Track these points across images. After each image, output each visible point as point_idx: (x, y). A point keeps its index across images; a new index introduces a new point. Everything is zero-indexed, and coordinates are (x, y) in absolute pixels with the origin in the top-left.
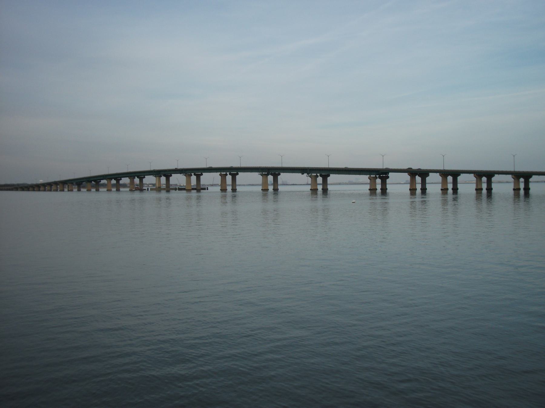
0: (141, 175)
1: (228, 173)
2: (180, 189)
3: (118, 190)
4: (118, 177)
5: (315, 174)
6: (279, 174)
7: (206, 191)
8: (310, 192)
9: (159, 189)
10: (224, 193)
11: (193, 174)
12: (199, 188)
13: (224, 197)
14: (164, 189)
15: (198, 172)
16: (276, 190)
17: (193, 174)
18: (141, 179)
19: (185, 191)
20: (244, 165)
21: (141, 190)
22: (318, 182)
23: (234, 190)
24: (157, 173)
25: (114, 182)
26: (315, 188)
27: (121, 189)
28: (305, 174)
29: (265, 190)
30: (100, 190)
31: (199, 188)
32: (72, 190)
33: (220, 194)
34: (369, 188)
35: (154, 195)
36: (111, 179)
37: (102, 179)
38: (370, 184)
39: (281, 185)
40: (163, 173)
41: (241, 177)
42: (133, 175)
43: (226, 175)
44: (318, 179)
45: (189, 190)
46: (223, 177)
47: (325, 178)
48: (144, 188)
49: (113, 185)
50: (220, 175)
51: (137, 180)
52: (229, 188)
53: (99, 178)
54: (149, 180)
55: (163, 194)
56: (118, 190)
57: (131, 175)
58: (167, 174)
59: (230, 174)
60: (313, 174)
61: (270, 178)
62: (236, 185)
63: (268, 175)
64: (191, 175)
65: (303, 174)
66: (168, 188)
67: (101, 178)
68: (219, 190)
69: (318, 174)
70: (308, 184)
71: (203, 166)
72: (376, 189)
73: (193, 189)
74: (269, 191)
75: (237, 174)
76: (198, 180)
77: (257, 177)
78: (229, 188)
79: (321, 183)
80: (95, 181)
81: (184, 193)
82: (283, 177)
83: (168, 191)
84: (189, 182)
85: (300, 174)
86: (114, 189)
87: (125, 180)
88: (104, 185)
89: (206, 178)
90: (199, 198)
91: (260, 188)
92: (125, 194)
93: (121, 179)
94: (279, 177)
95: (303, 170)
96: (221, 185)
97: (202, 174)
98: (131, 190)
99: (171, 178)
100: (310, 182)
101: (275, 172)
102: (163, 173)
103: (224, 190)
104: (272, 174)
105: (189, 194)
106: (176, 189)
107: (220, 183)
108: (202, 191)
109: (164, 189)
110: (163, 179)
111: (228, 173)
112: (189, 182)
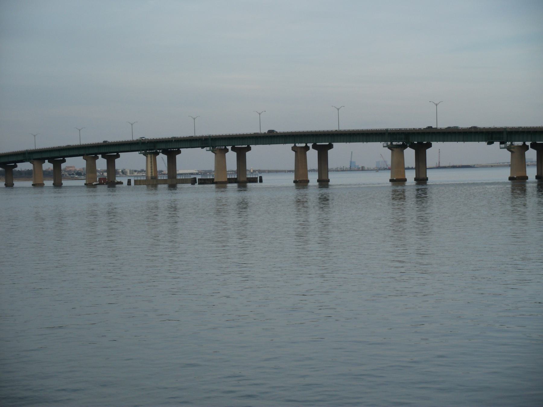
0: (111, 150)
1: (310, 145)
2: (203, 182)
3: (58, 185)
4: (57, 155)
5: (520, 143)
6: (429, 145)
7: (258, 184)
9: (152, 182)
11: (229, 148)
12: (242, 179)
15: (242, 143)
17: (229, 148)
19: (213, 186)
20: (443, 124)
22: (98, 168)
24: (149, 147)
25: (47, 166)
26: (520, 174)
27: (17, 184)
28: (497, 144)
29: (398, 181)
31: (243, 180)
33: (293, 193)
34: (389, 177)
35: (142, 197)
36: (42, 160)
37: (22, 161)
38: (511, 165)
39: (337, 170)
40: (163, 146)
42: (91, 151)
43: (307, 148)
44: (308, 153)
45: (221, 184)
47: (421, 152)
48: (118, 179)
49: (47, 175)
50: (294, 149)
51: (101, 163)
52: (313, 178)
53: (14, 159)
54: (131, 162)
56: (58, 185)
57: (89, 151)
58: (171, 147)
59: (233, 149)
61: (410, 154)
62: (327, 170)
63: (404, 147)
64: (227, 150)
65: (490, 143)
66: (173, 181)
68: (52, 185)
69: (528, 143)
72: (527, 178)
73: (231, 181)
74: (407, 183)
77: (379, 151)
78: (313, 178)
79: (413, 165)
83: (172, 187)
84: (221, 163)
85: (484, 144)
86: (49, 183)
87: (77, 163)
88: (27, 175)
89: (258, 157)
90: (243, 205)
91: (386, 176)
92: (75, 198)
93: (64, 161)
94: (428, 151)
95: (490, 135)
101: (419, 140)
104: (412, 146)
105: (220, 195)
108: (249, 185)
109: (164, 182)
111: (310, 145)
112: (221, 163)
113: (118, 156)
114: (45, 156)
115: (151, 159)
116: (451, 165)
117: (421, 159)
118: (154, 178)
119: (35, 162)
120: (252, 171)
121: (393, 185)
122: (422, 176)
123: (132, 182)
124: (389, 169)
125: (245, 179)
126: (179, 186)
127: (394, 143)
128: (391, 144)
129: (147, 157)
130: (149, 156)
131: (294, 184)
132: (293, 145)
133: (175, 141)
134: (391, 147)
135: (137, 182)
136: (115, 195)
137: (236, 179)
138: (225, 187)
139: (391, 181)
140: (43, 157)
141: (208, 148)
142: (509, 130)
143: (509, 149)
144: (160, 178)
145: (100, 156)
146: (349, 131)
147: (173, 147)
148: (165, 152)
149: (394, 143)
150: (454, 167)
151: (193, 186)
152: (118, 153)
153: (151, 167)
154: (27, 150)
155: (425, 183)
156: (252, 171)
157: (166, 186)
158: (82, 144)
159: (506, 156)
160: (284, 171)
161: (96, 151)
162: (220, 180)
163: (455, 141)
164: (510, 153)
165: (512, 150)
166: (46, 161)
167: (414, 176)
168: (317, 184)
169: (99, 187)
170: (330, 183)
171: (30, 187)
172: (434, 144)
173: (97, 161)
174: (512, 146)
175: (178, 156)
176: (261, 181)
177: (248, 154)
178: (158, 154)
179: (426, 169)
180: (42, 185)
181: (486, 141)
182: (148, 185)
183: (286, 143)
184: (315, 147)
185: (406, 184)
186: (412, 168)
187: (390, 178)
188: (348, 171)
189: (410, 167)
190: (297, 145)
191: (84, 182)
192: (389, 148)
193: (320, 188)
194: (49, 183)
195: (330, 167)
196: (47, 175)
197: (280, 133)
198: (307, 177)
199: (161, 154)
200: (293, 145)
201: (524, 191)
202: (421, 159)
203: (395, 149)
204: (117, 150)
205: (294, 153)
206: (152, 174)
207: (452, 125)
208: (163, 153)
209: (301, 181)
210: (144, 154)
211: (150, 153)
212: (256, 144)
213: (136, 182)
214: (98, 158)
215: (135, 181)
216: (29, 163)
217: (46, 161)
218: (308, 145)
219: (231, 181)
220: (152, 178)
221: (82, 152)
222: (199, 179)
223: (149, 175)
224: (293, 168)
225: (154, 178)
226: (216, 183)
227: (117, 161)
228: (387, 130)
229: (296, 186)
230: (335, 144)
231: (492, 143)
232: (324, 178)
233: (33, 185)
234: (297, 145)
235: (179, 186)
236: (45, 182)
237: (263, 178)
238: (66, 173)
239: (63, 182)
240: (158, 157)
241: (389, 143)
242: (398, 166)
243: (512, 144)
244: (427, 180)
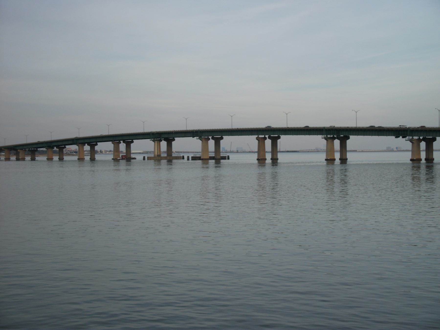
1: (210, 137)
3: (33, 159)
5: (263, 136)
10: (331, 167)
11: (210, 137)
14: (165, 158)
15: (217, 135)
22: (121, 150)
27: (66, 158)
30: (37, 158)
31: (170, 158)
32: (23, 159)
36: (84, 144)
38: (413, 151)
40: (166, 136)
43: (265, 138)
44: (266, 141)
46: (261, 141)
47: (430, 143)
48: (133, 156)
50: (257, 139)
51: (122, 146)
58: (169, 137)
59: (212, 138)
62: (277, 152)
63: (334, 138)
64: (209, 139)
69: (267, 136)
73: (211, 158)
74: (267, 162)
76: (217, 145)
80: (57, 147)
82: (353, 141)
84: (205, 147)
85: (394, 137)
93: (97, 145)
96: (259, 152)
99: (132, 145)
104: (338, 138)
107: (256, 150)
109: (165, 158)
113: (132, 142)
116: (287, 150)
118: (159, 156)
119: (80, 145)
124: (267, 152)
125: (219, 157)
127: (329, 136)
128: (327, 136)
130: (156, 142)
132: (257, 136)
134: (326, 139)
135: (149, 158)
136: (160, 169)
137: (214, 157)
139: (326, 160)
141: (198, 138)
145: (122, 142)
146: (297, 128)
148: (166, 139)
149: (329, 136)
150: (288, 152)
152: (132, 140)
155: (432, 162)
159: (409, 145)
164: (411, 143)
170: (279, 161)
171: (75, 161)
175: (173, 143)
176: (228, 159)
177: (221, 141)
178: (161, 141)
179: (277, 152)
181: (394, 136)
184: (270, 138)
185: (348, 163)
187: (325, 158)
190: (260, 136)
200: (257, 136)
201: (419, 167)
205: (257, 141)
207: (380, 126)
208: (164, 140)
209: (262, 159)
210: (153, 141)
211: (157, 140)
212: (285, 134)
214: (121, 143)
215: (148, 157)
217: (86, 144)
219: (211, 158)
221: (111, 139)
222: (192, 157)
223: (156, 154)
225: (159, 156)
226: (202, 159)
228: (324, 128)
229: (259, 163)
231: (399, 137)
232: (275, 157)
234: (260, 136)
235: (174, 161)
240: (161, 143)
242: (330, 150)
243: (413, 138)
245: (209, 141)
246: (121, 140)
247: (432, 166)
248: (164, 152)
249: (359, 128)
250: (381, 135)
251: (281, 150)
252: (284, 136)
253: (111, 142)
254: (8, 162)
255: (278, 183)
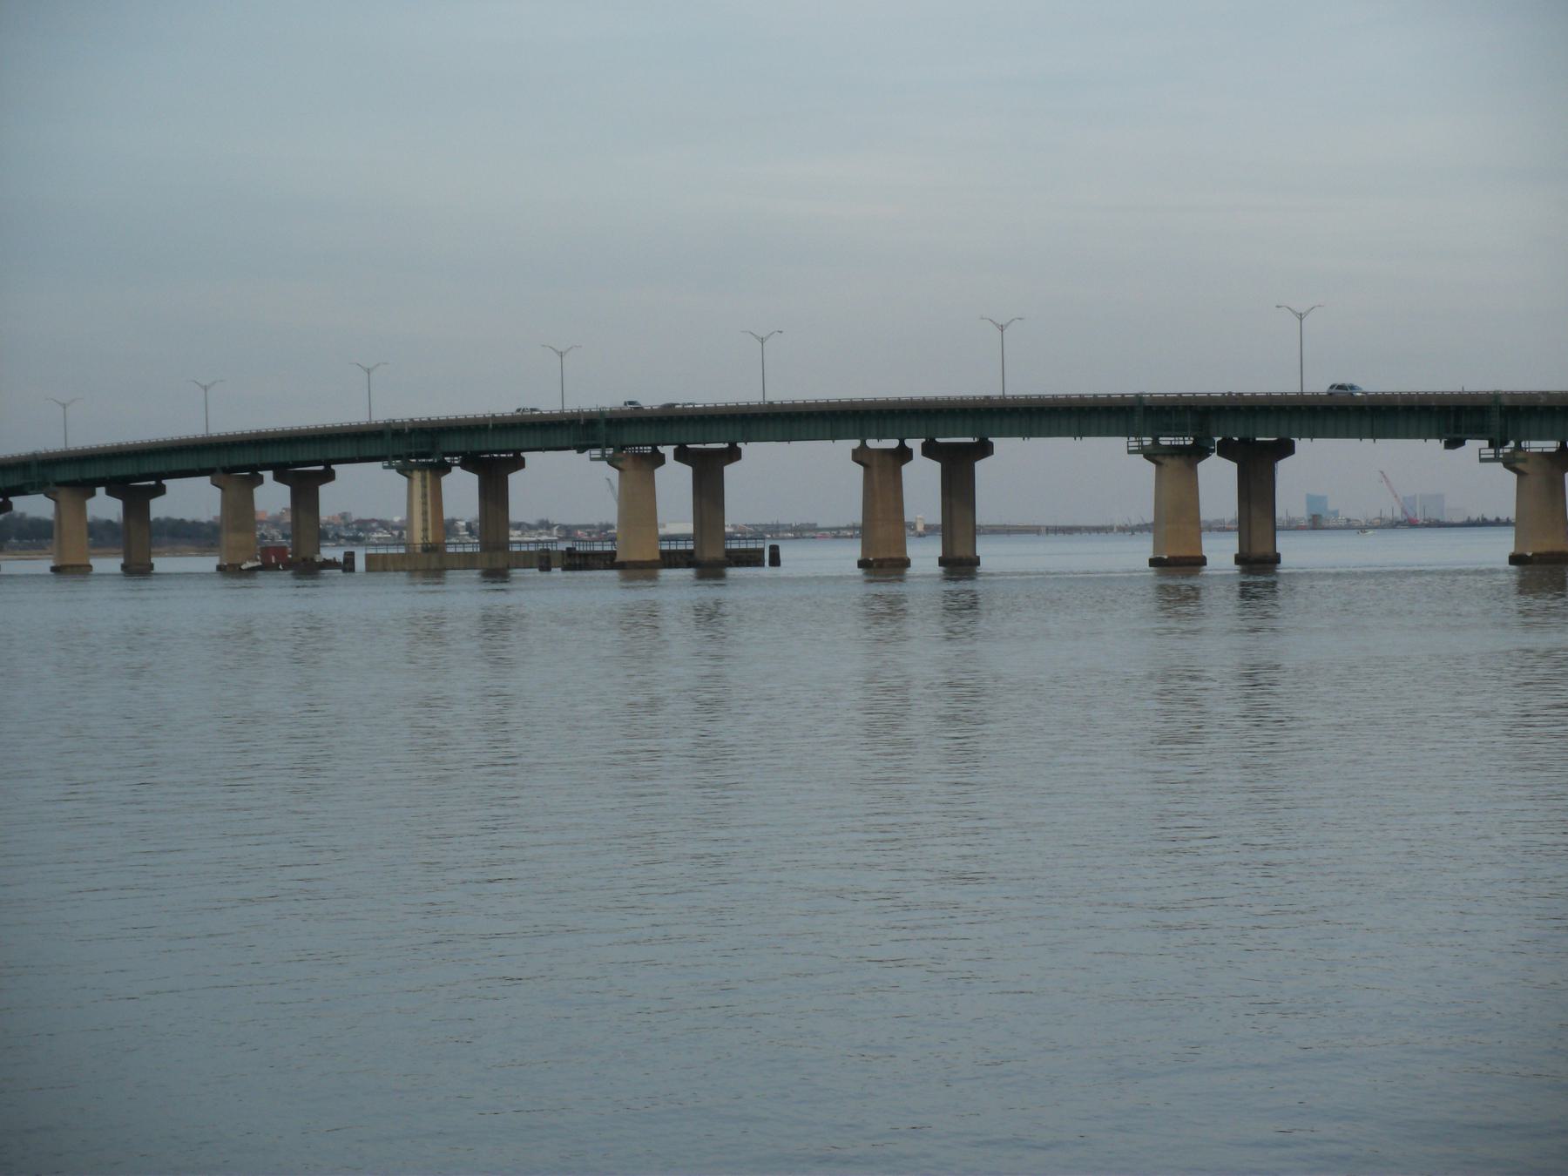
0: (305, 457)
1: (915, 444)
2: (577, 561)
3: (138, 569)
4: (134, 471)
6: (1286, 449)
7: (767, 571)
8: (1510, 576)
9: (429, 561)
11: (668, 451)
12: (712, 553)
13: (895, 609)
15: (709, 437)
16: (1258, 562)
17: (668, 451)
18: (305, 491)
19: (614, 574)
21: (307, 568)
23: (959, 565)
24: (420, 447)
25: (105, 507)
28: (1475, 447)
30: (161, 564)
32: (83, 570)
33: (859, 589)
35: (397, 598)
36: (86, 488)
37: (20, 491)
38: (1519, 524)
41: (1012, 471)
43: (904, 454)
44: (906, 469)
46: (882, 475)
47: (959, 472)
49: (101, 535)
50: (860, 456)
51: (272, 497)
52: (924, 555)
54: (364, 492)
55: (464, 595)
56: (138, 569)
57: (233, 459)
58: (491, 448)
59: (682, 455)
60: (1535, 446)
61: (1218, 478)
62: (973, 531)
64: (659, 460)
65: (1454, 443)
66: (496, 555)
67: (14, 480)
70: (837, 534)
71: (741, 392)
73: (672, 560)
75: (984, 449)
76: (708, 492)
77: (1116, 472)
79: (936, 518)
81: (601, 592)
82: (1312, 469)
85: (1436, 445)
86: (110, 564)
87: (190, 499)
88: (35, 535)
89: (763, 481)
90: (495, 625)
91: (1140, 552)
93: (160, 491)
97: (733, 454)
98: (228, 570)
100: (1509, 511)
101: (1254, 432)
102: (459, 444)
103: (884, 564)
104: (1226, 450)
106: (544, 561)
108: (732, 572)
109: (467, 562)
110: (461, 491)
111: (915, 444)
113: (329, 476)
114: (92, 472)
115: (424, 486)
117: (1256, 492)
119: (64, 494)
120: (920, 528)
121: (1159, 574)
122: (1259, 549)
123: (360, 564)
125: (720, 555)
126: (516, 573)
128: (1156, 441)
129: (410, 478)
130: (417, 475)
131: (860, 572)
132: (856, 443)
133: (496, 427)
137: (691, 553)
138: (654, 578)
140: (87, 476)
141: (596, 453)
142: (1506, 402)
143: (1509, 463)
144: (450, 550)
146: (1028, 399)
147: (497, 447)
148: (471, 462)
151: (545, 574)
152: (328, 463)
153: (425, 513)
154: (34, 455)
156: (920, 528)
157: (474, 574)
158: (1310, 388)
160: (1035, 530)
161: (251, 457)
162: (635, 556)
163: (1418, 437)
164: (1513, 477)
165: (1519, 466)
166: (101, 491)
167: (937, 550)
168: (939, 570)
169: (264, 579)
170: (980, 569)
172: (1301, 444)
173: (258, 492)
174: (1520, 455)
175: (514, 479)
176: (775, 561)
178: (446, 468)
180: (83, 570)
181: (1439, 437)
182: (412, 572)
183: (1081, 435)
184: (930, 450)
186: (1507, 523)
188: (1300, 528)
189: (1503, 517)
190: (872, 444)
191: (51, 563)
192: (1148, 456)
193: (1520, 593)
194: (110, 564)
195: (1280, 513)
196: (101, 535)
197: (782, 405)
198: (904, 550)
199: (456, 470)
200: (856, 443)
202: (1256, 492)
203: (1167, 461)
204: (517, 446)
206: (425, 537)
208: (464, 466)
210: (401, 471)
211: (422, 468)
213: (374, 564)
214: (260, 481)
216: (42, 496)
217: (101, 491)
218: (909, 443)
220: (428, 549)
221: (208, 461)
223: (418, 538)
224: (855, 515)
226: (621, 566)
227: (325, 490)
230: (999, 443)
233: (54, 569)
234: (872, 444)
236: (92, 562)
237: (783, 554)
238: (274, 532)
239: (154, 560)
241: (1147, 441)
243: (1518, 447)
244: (1278, 561)
245: (659, 473)
246: (266, 468)
247: (1274, 583)
248: (275, 522)
249: (1015, 399)
250: (1325, 434)
251: (1291, 521)
252: (1016, 442)
253: (207, 479)
254: (68, 589)
255: (660, 624)
